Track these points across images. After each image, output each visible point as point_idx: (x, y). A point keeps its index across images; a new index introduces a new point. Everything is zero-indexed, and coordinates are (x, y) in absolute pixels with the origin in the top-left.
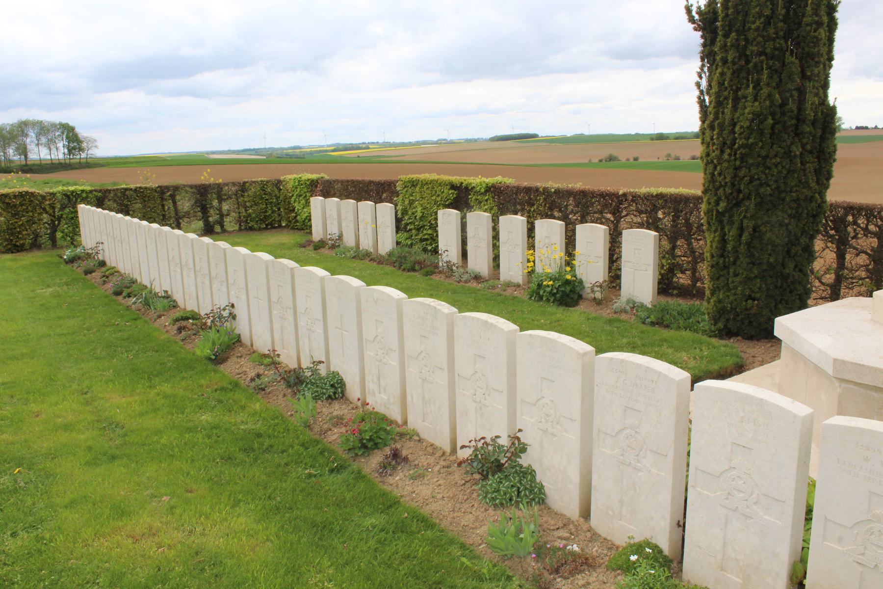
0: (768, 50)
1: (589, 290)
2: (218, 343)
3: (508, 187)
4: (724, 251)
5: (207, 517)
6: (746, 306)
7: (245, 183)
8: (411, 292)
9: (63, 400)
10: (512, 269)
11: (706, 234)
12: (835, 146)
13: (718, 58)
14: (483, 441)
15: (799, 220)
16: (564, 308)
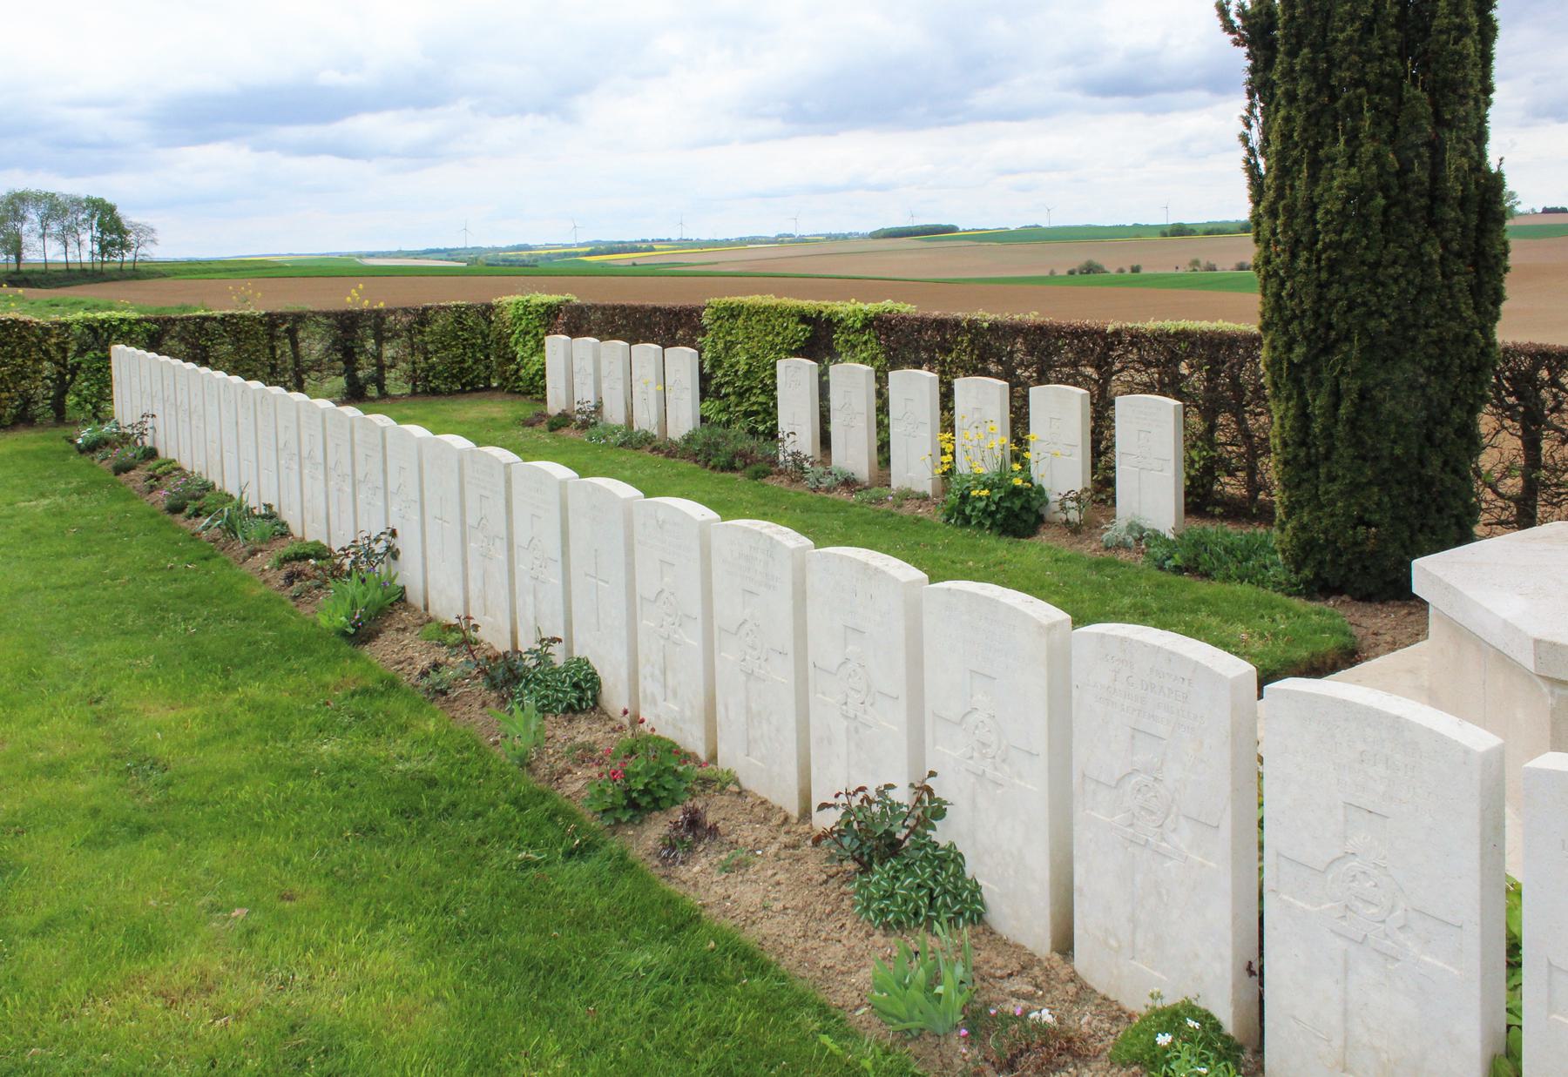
0: (1370, 77)
1: (1056, 507)
2: (361, 602)
3: (904, 318)
4: (1307, 434)
5: (319, 952)
6: (1354, 535)
7: (426, 309)
8: (726, 509)
9: (51, 715)
10: (914, 468)
11: (1272, 404)
12: (1505, 244)
13: (1279, 92)
14: (861, 795)
15: (1445, 378)
16: (1010, 539)
